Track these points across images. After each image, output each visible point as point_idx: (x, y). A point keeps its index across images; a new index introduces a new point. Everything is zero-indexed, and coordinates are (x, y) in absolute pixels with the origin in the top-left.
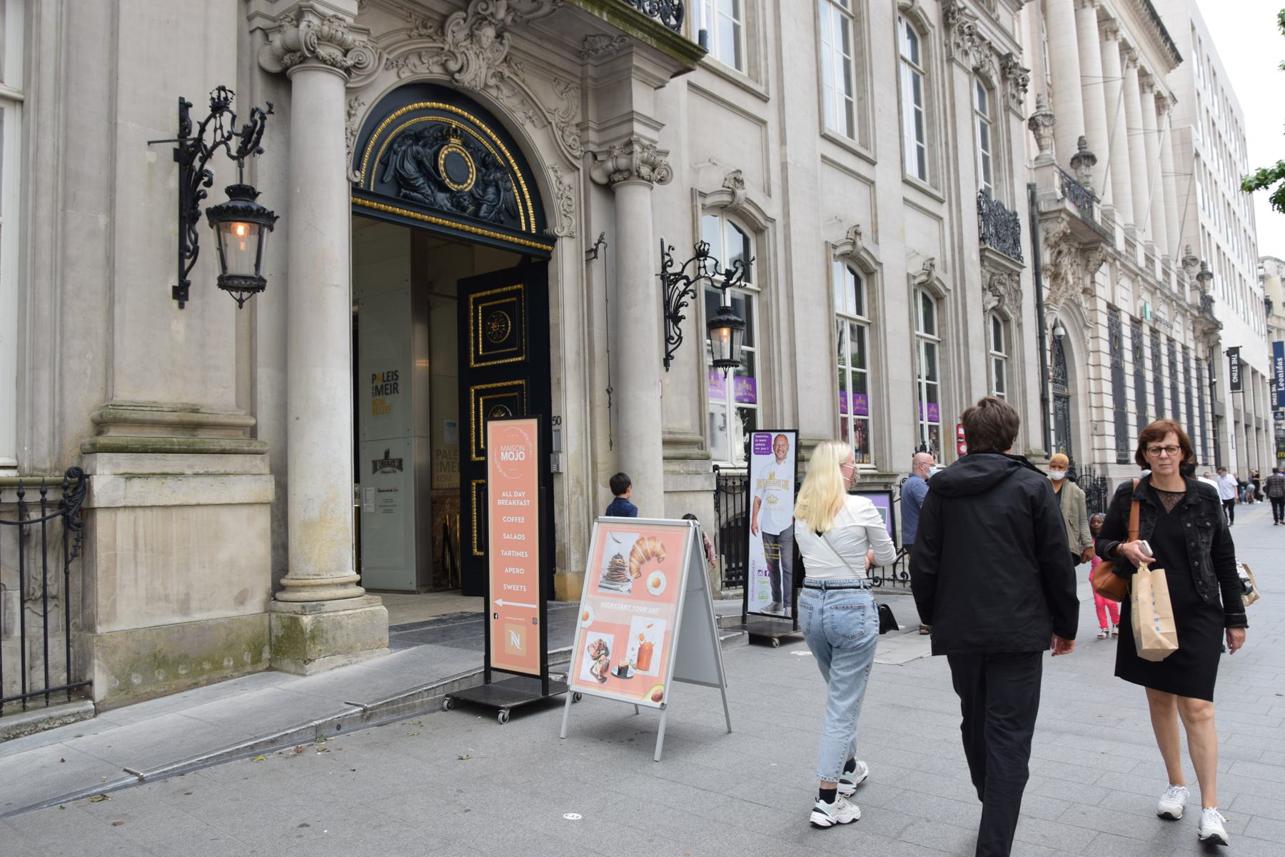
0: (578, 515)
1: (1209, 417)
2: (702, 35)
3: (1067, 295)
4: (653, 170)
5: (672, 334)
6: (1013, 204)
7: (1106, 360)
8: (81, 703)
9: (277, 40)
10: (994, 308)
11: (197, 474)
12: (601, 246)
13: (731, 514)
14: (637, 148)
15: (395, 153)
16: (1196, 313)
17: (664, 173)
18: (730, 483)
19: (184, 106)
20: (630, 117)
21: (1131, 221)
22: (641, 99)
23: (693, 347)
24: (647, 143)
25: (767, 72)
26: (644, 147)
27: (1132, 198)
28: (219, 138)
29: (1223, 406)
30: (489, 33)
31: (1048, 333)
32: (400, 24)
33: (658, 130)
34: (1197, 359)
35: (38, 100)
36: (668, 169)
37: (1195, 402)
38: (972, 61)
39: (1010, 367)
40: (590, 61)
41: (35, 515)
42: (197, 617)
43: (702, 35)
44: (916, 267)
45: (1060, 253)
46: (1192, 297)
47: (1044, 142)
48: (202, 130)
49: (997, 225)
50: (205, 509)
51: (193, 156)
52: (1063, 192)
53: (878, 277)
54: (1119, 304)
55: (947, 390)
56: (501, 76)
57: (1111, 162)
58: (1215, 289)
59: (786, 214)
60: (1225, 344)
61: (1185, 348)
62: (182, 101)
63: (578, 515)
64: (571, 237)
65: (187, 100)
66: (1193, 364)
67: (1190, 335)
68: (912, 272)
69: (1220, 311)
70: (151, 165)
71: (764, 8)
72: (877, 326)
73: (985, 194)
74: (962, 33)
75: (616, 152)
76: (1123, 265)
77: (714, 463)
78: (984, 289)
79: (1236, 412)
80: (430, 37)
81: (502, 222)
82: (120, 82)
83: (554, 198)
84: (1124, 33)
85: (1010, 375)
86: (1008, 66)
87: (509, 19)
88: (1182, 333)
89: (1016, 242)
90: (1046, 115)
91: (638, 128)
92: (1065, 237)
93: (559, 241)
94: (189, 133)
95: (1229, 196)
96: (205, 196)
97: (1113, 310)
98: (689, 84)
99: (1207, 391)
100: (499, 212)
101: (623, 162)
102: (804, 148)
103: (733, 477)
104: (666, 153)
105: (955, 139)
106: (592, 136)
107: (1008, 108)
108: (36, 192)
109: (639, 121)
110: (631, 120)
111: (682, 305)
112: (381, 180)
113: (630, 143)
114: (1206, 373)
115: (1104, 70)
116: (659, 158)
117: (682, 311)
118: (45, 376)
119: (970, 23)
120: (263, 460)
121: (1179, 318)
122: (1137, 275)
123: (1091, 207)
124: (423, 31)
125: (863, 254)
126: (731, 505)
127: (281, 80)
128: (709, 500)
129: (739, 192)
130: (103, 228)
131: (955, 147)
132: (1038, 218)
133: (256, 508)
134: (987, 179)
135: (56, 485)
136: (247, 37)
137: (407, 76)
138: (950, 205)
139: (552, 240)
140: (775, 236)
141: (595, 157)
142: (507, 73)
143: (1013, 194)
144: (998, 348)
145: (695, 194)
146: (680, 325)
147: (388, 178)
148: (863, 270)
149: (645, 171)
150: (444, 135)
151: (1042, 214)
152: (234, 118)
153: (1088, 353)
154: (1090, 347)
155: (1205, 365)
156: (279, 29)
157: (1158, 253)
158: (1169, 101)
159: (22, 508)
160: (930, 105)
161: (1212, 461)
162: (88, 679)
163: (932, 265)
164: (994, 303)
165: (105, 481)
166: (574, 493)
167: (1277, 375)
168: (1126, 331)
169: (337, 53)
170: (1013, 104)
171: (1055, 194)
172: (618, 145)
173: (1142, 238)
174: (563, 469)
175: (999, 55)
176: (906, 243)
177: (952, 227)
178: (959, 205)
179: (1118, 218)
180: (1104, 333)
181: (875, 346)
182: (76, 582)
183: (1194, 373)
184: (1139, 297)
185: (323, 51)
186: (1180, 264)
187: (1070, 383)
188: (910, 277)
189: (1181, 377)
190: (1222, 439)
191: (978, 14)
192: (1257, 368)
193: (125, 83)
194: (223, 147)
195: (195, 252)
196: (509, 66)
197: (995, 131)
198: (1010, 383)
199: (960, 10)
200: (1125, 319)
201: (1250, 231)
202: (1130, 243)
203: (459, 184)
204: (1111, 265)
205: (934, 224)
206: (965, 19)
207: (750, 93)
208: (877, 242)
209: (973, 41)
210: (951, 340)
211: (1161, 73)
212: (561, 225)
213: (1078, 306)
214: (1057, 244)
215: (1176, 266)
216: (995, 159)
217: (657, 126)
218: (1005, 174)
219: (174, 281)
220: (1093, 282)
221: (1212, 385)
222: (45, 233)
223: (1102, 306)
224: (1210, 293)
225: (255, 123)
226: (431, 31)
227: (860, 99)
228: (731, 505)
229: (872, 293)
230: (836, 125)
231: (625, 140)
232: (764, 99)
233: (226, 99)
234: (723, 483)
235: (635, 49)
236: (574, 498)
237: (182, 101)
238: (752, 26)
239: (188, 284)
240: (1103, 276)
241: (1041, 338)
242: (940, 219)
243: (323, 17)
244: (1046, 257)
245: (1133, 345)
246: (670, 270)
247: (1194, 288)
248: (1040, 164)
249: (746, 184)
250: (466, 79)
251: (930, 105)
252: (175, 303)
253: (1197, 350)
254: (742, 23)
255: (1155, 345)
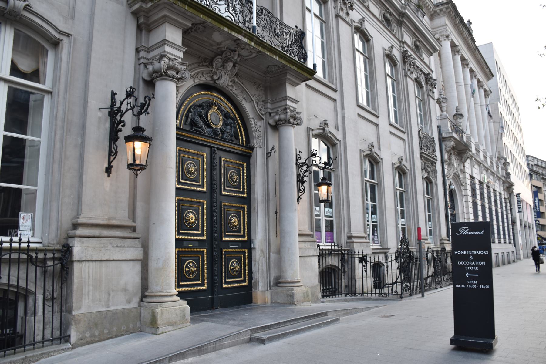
0: (262, 266)
1: (510, 223)
2: (314, 65)
3: (454, 172)
4: (295, 120)
5: (301, 188)
6: (432, 135)
7: (470, 199)
8: (65, 344)
9: (150, 68)
10: (426, 177)
11: (117, 246)
12: (273, 151)
13: (324, 265)
14: (288, 111)
15: (191, 112)
16: (504, 179)
17: (299, 121)
18: (324, 252)
19: (113, 94)
20: (286, 98)
21: (477, 141)
22: (290, 91)
23: (308, 194)
24: (292, 109)
25: (336, 80)
26: (291, 111)
27: (476, 132)
28: (129, 107)
29: (515, 217)
30: (231, 64)
31: (448, 187)
32: (195, 61)
33: (296, 103)
34: (505, 198)
35: (59, 92)
36: (300, 119)
37: (505, 217)
38: (414, 76)
39: (433, 202)
40: (269, 75)
41: (50, 263)
42: (112, 308)
43: (314, 65)
44: (395, 160)
45: (451, 154)
46: (501, 173)
47: (443, 109)
48: (122, 103)
49: (426, 142)
50: (116, 262)
51: (117, 114)
52: (452, 129)
53: (381, 164)
54: (474, 176)
55: (408, 212)
56: (234, 81)
57: (469, 118)
58: (511, 169)
59: (345, 138)
60: (515, 192)
61: (500, 194)
62: (112, 92)
63: (262, 266)
64: (260, 147)
65: (114, 92)
66: (503, 200)
67: (502, 188)
68: (393, 162)
69: (513, 178)
70: (100, 118)
71: (335, 55)
72: (381, 185)
73: (421, 129)
74: (410, 65)
75: (280, 113)
76: (475, 159)
77: (318, 244)
78: (422, 170)
79: (521, 220)
80: (207, 66)
81: (232, 141)
82: (90, 84)
83: (253, 131)
84: (471, 65)
85: (433, 205)
86: (428, 78)
87: (239, 60)
88: (499, 188)
89: (434, 150)
90: (444, 98)
91: (289, 103)
92: (453, 148)
93: (255, 149)
94: (115, 105)
95: (514, 131)
96: (121, 131)
97: (472, 177)
98: (306, 85)
99: (509, 212)
100: (232, 136)
101: (283, 116)
102: (351, 111)
103: (325, 250)
104: (300, 113)
105: (409, 107)
106: (269, 105)
107: (429, 95)
108: (56, 129)
109: (289, 100)
110: (286, 99)
111: (305, 176)
112: (185, 124)
113: (286, 109)
114: (508, 204)
115: (464, 79)
116: (297, 115)
117: (305, 179)
118: (55, 204)
119: (413, 61)
120: (139, 241)
121: (497, 181)
122: (481, 163)
123: (462, 135)
124: (205, 64)
125: (375, 154)
126: (324, 261)
127: (150, 84)
128: (316, 259)
129: (327, 129)
130: (80, 143)
131: (409, 111)
132: (442, 140)
133: (136, 262)
134: (421, 124)
135: (58, 251)
136: (138, 66)
137: (197, 81)
138: (408, 134)
139: (252, 148)
140: (340, 147)
141: (270, 114)
142: (236, 80)
143: (432, 130)
144: (428, 194)
145: (309, 130)
146: (304, 185)
147: (188, 122)
148: (373, 160)
149: (292, 120)
150: (210, 105)
151: (444, 138)
152: (136, 99)
153: (463, 196)
154: (464, 193)
155: (508, 201)
156: (151, 63)
157: (488, 154)
158: (489, 92)
159: (45, 260)
160: (399, 94)
161: (512, 241)
162: (68, 333)
163: (402, 159)
164: (426, 175)
165: (78, 249)
166: (260, 257)
167: (535, 205)
168: (477, 187)
169: (174, 73)
170: (431, 93)
171: (448, 130)
172: (280, 109)
173: (482, 148)
174: (256, 246)
175: (424, 74)
176: (391, 152)
177: (409, 144)
178: (411, 134)
179: (472, 140)
180: (469, 188)
181: (380, 193)
182: (64, 293)
183: (504, 204)
184: (482, 173)
185: (169, 72)
186: (496, 159)
187: (456, 209)
188: (361, 151)
189: (499, 206)
190: (515, 232)
191: (416, 57)
192: (524, 199)
193: (92, 85)
194: (130, 111)
195: (116, 153)
196: (237, 77)
197: (424, 104)
198: (433, 209)
199: (409, 56)
200: (477, 182)
201: (522, 145)
202: (477, 151)
203: (216, 125)
204: (471, 160)
205: (402, 142)
206: (411, 59)
207: (332, 88)
208: (380, 149)
209: (414, 68)
210: (410, 191)
211: (485, 81)
212: (256, 142)
213: (459, 176)
214: (450, 151)
215: (495, 160)
216: (425, 116)
217: (296, 102)
218: (428, 122)
219: (106, 165)
220: (464, 166)
221: (511, 209)
222: (58, 145)
223: (468, 176)
224: (509, 171)
225: (146, 102)
226: (208, 63)
227: (371, 91)
228: (324, 261)
229: (379, 171)
230: (363, 101)
231: (283, 108)
232: (335, 91)
233: (133, 91)
234: (321, 252)
235: (288, 71)
236: (261, 259)
237: (112, 92)
238: (330, 62)
239: (112, 167)
240: (468, 164)
241: (445, 190)
242: (404, 140)
243: (170, 59)
244: (446, 156)
245: (480, 193)
246: (300, 161)
247: (502, 169)
248: (442, 118)
249: (329, 126)
250: (221, 82)
251: (399, 94)
252: (106, 174)
253: (505, 195)
254: (326, 60)
255: (489, 193)
